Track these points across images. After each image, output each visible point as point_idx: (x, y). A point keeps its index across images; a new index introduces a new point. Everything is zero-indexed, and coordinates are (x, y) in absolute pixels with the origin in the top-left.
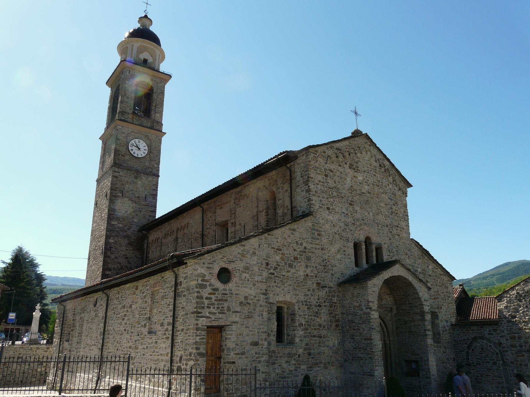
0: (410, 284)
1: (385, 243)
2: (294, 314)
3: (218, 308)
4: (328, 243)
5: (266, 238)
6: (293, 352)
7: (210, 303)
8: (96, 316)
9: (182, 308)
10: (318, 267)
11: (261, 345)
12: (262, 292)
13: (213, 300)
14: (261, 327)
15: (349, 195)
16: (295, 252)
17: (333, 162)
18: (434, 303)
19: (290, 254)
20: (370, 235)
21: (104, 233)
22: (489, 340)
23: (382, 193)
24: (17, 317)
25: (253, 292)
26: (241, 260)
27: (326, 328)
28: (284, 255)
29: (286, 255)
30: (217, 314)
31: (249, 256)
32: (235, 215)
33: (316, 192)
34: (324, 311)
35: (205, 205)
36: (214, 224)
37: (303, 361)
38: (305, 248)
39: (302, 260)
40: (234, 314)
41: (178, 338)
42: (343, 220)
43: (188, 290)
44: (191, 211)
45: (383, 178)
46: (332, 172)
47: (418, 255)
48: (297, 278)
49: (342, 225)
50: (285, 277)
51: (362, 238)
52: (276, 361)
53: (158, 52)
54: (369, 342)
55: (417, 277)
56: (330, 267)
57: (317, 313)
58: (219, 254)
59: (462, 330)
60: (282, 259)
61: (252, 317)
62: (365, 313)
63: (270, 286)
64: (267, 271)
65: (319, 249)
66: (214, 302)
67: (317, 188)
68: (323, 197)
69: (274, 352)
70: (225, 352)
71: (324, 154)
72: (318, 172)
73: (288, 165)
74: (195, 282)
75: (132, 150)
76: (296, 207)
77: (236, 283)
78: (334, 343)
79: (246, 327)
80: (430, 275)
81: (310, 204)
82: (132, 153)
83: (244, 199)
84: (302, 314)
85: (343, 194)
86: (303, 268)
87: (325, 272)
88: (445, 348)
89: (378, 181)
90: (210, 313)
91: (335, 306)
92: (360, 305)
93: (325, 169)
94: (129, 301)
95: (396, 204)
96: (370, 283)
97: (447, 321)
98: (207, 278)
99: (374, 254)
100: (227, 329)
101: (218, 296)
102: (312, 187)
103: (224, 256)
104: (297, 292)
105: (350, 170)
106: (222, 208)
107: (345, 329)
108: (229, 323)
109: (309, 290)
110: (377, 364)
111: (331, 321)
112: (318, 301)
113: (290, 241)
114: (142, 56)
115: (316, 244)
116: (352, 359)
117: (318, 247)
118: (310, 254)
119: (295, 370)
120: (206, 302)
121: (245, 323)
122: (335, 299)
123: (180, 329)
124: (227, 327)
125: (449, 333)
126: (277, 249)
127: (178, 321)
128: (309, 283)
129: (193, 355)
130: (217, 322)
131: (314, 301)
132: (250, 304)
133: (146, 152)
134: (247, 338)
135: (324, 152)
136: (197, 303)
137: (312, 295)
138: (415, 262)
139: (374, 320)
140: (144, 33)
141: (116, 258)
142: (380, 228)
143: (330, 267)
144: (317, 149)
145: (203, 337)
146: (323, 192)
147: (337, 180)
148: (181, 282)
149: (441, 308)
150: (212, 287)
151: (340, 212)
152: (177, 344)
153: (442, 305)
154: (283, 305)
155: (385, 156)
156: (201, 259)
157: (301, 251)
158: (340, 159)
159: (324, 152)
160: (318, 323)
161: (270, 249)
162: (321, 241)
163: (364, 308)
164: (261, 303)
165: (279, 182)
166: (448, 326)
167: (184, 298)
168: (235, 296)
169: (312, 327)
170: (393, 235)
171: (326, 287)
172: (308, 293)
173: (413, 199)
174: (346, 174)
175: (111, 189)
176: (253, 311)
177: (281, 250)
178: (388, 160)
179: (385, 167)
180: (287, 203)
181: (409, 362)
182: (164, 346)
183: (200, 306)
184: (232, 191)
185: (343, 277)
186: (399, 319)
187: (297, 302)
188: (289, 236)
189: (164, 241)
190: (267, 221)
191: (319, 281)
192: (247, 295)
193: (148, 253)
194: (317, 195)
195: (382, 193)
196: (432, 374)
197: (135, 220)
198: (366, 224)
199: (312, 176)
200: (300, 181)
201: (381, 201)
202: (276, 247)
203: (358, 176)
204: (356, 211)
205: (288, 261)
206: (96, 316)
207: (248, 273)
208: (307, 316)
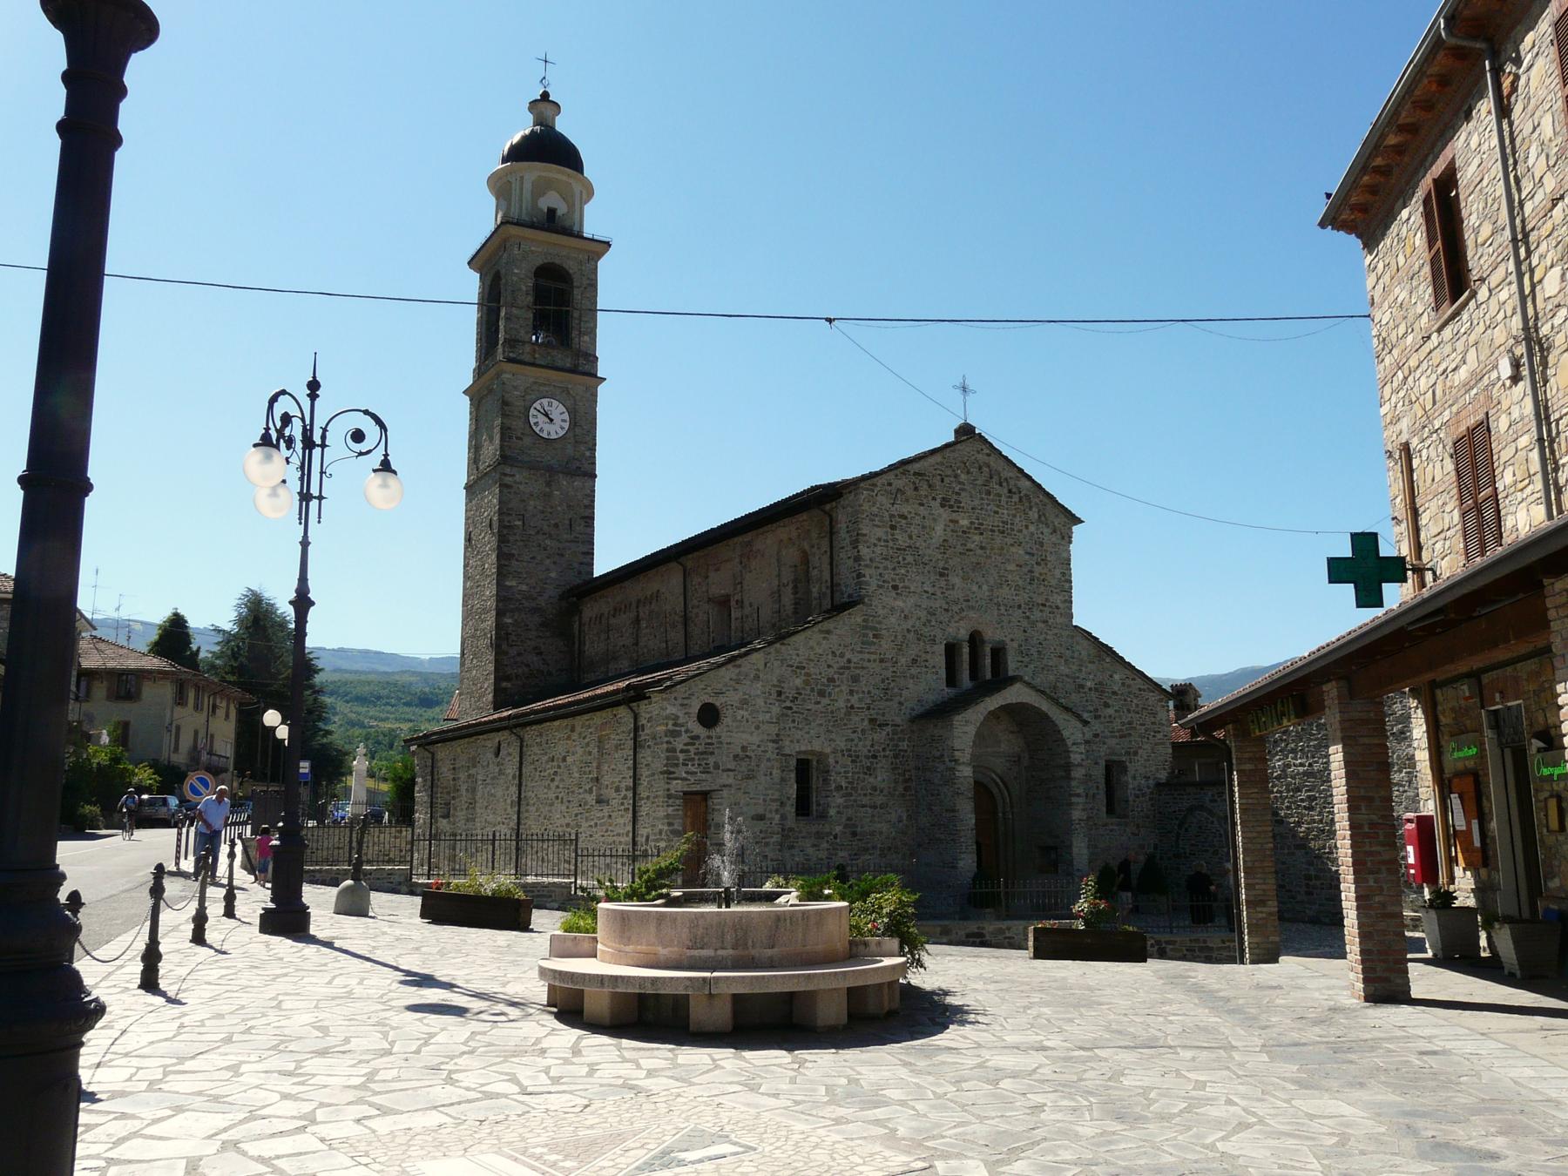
5: (777, 651)
8: (501, 772)
21: (491, 603)
22: (1210, 812)
24: (312, 767)
25: (755, 739)
31: (748, 689)
35: (689, 561)
44: (663, 569)
49: (923, 614)
51: (964, 634)
53: (577, 188)
55: (1056, 701)
60: (806, 683)
68: (886, 568)
69: (791, 829)
73: (828, 507)
75: (536, 424)
80: (1114, 693)
81: (860, 583)
82: (537, 430)
93: (892, 516)
94: (560, 750)
95: (1043, 561)
96: (958, 719)
98: (681, 721)
99: (988, 661)
102: (864, 551)
104: (833, 736)
114: (544, 204)
117: (873, 657)
120: (681, 756)
122: (904, 745)
128: (856, 719)
131: (863, 748)
133: (566, 426)
136: (668, 758)
140: (546, 148)
141: (519, 654)
149: (1136, 753)
155: (1021, 471)
164: (768, 755)
165: (814, 535)
170: (1033, 624)
175: (501, 512)
178: (1029, 478)
182: (622, 821)
183: (672, 762)
189: (612, 621)
193: (582, 643)
197: (553, 575)
198: (972, 608)
206: (501, 772)
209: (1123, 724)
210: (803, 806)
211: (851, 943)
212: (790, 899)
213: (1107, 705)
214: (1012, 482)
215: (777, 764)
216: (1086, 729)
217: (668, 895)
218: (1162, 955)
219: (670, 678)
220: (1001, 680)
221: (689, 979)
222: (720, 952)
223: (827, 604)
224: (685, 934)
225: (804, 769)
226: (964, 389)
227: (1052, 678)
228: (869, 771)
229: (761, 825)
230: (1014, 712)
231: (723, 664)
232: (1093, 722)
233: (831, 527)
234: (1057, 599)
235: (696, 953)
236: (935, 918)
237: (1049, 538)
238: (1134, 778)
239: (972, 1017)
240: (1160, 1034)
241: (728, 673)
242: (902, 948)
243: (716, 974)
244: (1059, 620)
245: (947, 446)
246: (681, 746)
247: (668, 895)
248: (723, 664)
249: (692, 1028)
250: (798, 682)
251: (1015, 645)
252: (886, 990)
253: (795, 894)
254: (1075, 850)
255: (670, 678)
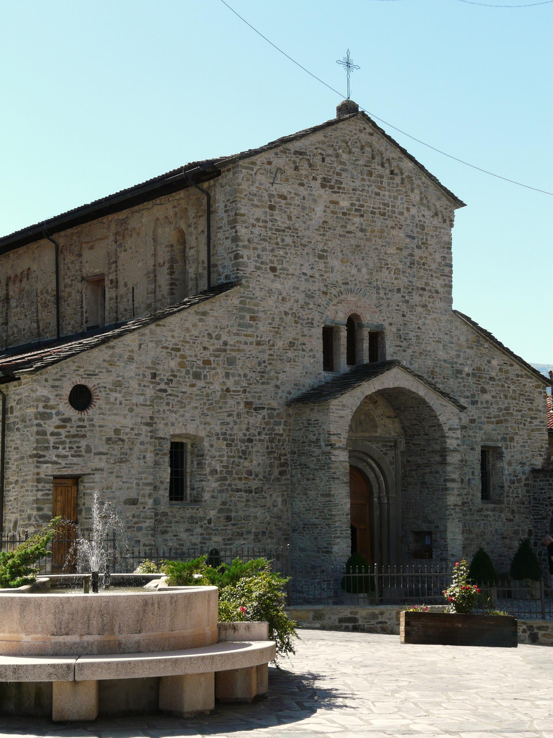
0: (422, 402)
1: (391, 324)
2: (202, 455)
3: (71, 448)
4: (270, 331)
5: (152, 332)
6: (199, 515)
7: (58, 440)
9: (15, 448)
10: (250, 374)
11: (142, 503)
12: (144, 421)
13: (63, 436)
14: (143, 476)
15: (319, 238)
16: (205, 352)
17: (287, 180)
18: (495, 430)
19: (196, 356)
20: (359, 312)
23: (392, 228)
25: (128, 422)
26: (109, 371)
27: (261, 477)
28: (186, 358)
29: (189, 359)
30: (70, 458)
31: (122, 366)
32: (117, 266)
33: (249, 241)
34: (258, 448)
35: (61, 238)
36: (79, 278)
37: (217, 530)
38: (225, 344)
39: (218, 364)
40: (98, 457)
41: (11, 493)
42: (302, 289)
43: (24, 421)
44: (33, 245)
45: (395, 198)
46: (285, 198)
47: (467, 340)
48: (207, 395)
49: (301, 297)
50: (187, 394)
51: (342, 318)
52: (169, 529)
54: (327, 499)
55: (435, 389)
56: (273, 373)
57: (244, 452)
58: (71, 363)
59: (548, 481)
61: (127, 461)
62: (324, 453)
63: (159, 411)
64: (154, 388)
65: (251, 343)
66: (64, 439)
67: (252, 233)
68: (264, 249)
69: (165, 514)
70: (83, 513)
71: (268, 167)
72: (256, 202)
73: (206, 185)
74: (34, 410)
76: (216, 266)
77: (100, 408)
78: (275, 501)
79: (117, 477)
80: (492, 379)
83: (131, 236)
84: (218, 454)
85: (305, 239)
86: (221, 378)
87: (263, 383)
88: (513, 512)
89: (384, 204)
90: (58, 456)
91: (279, 440)
92: (318, 440)
93: (271, 196)
96: (334, 403)
97: (523, 464)
98: (52, 403)
99: (366, 345)
100: (85, 481)
101: (71, 430)
102: (242, 231)
103: (79, 367)
104: (208, 419)
105: (322, 191)
106: (92, 248)
107: (295, 480)
108: (87, 472)
109: (230, 415)
110: (338, 535)
111: (271, 466)
112: (248, 433)
113: (196, 333)
115: (246, 335)
116: (304, 528)
118: (234, 354)
119: (201, 543)
120: (52, 439)
121: (115, 470)
122: (280, 429)
123: (13, 481)
124: (86, 477)
125: (526, 485)
126: (173, 349)
127: (10, 468)
128: (231, 402)
129: (33, 519)
130: (70, 470)
131: (239, 433)
132: (123, 441)
134: (118, 493)
135: (270, 163)
136: (37, 441)
137: (235, 423)
138: (458, 356)
139: (336, 465)
142: (382, 295)
143: (273, 373)
144: (253, 159)
145: (47, 492)
146: (265, 240)
147: (295, 212)
148: (12, 407)
149: (512, 439)
150: (60, 417)
151: (297, 272)
152: (9, 503)
153: (516, 434)
154: (184, 441)
155: (404, 151)
156: (41, 374)
157: (218, 350)
158: (303, 172)
159: (270, 163)
160: (245, 469)
161: (159, 349)
162: (257, 328)
163: (323, 444)
164: (142, 438)
165: (192, 213)
166: (524, 473)
167: (18, 433)
168: (98, 429)
169: (234, 476)
171: (264, 408)
172: (229, 419)
173: (464, 230)
174: (315, 201)
176: (129, 452)
177: (179, 350)
178: (412, 159)
179: (402, 174)
180: (203, 256)
181: (420, 535)
184: (110, 217)
185: (299, 390)
186: (409, 461)
187: (208, 436)
188: (195, 325)
190: (172, 284)
191: (251, 400)
192: (118, 427)
194: (252, 246)
195: (392, 228)
196: (450, 553)
198: (351, 291)
199: (242, 212)
200: (222, 219)
201: (389, 243)
202: (170, 347)
203: (339, 199)
204: (332, 268)
205: (192, 367)
207: (120, 392)
208: (225, 458)
209: (500, 410)
210: (177, 490)
211: (220, 627)
212: (159, 584)
213: (484, 391)
214: (394, 164)
215: (151, 448)
216: (463, 415)
217: (33, 580)
218: (534, 640)
219: (41, 359)
220: (378, 364)
221: (53, 666)
222: (86, 638)
223: (203, 285)
224: (49, 619)
225: (177, 452)
226: (348, 64)
227: (429, 363)
228: (245, 455)
229: (132, 510)
230: (392, 397)
231: (93, 347)
232: (470, 407)
233: (209, 205)
234: (437, 283)
235: (60, 639)
236: (307, 602)
237: (431, 222)
238: (510, 464)
239: (339, 701)
240: (525, 718)
241: (101, 355)
242: (271, 632)
243: (80, 661)
244: (440, 305)
245: (329, 124)
246: (51, 429)
247: (33, 580)
248: (93, 347)
249: (55, 716)
250: (173, 364)
251: (394, 329)
252: (254, 676)
253: (164, 579)
254: (449, 536)
255: (41, 359)
